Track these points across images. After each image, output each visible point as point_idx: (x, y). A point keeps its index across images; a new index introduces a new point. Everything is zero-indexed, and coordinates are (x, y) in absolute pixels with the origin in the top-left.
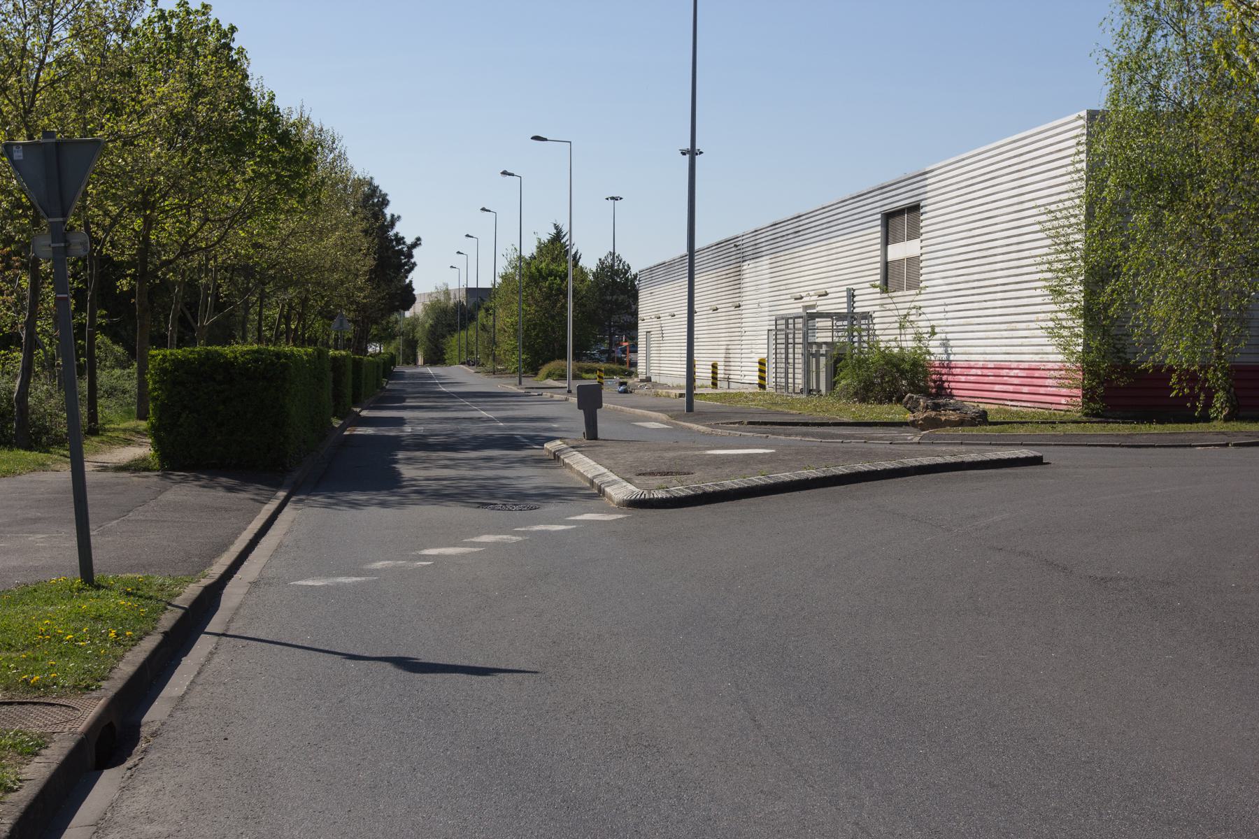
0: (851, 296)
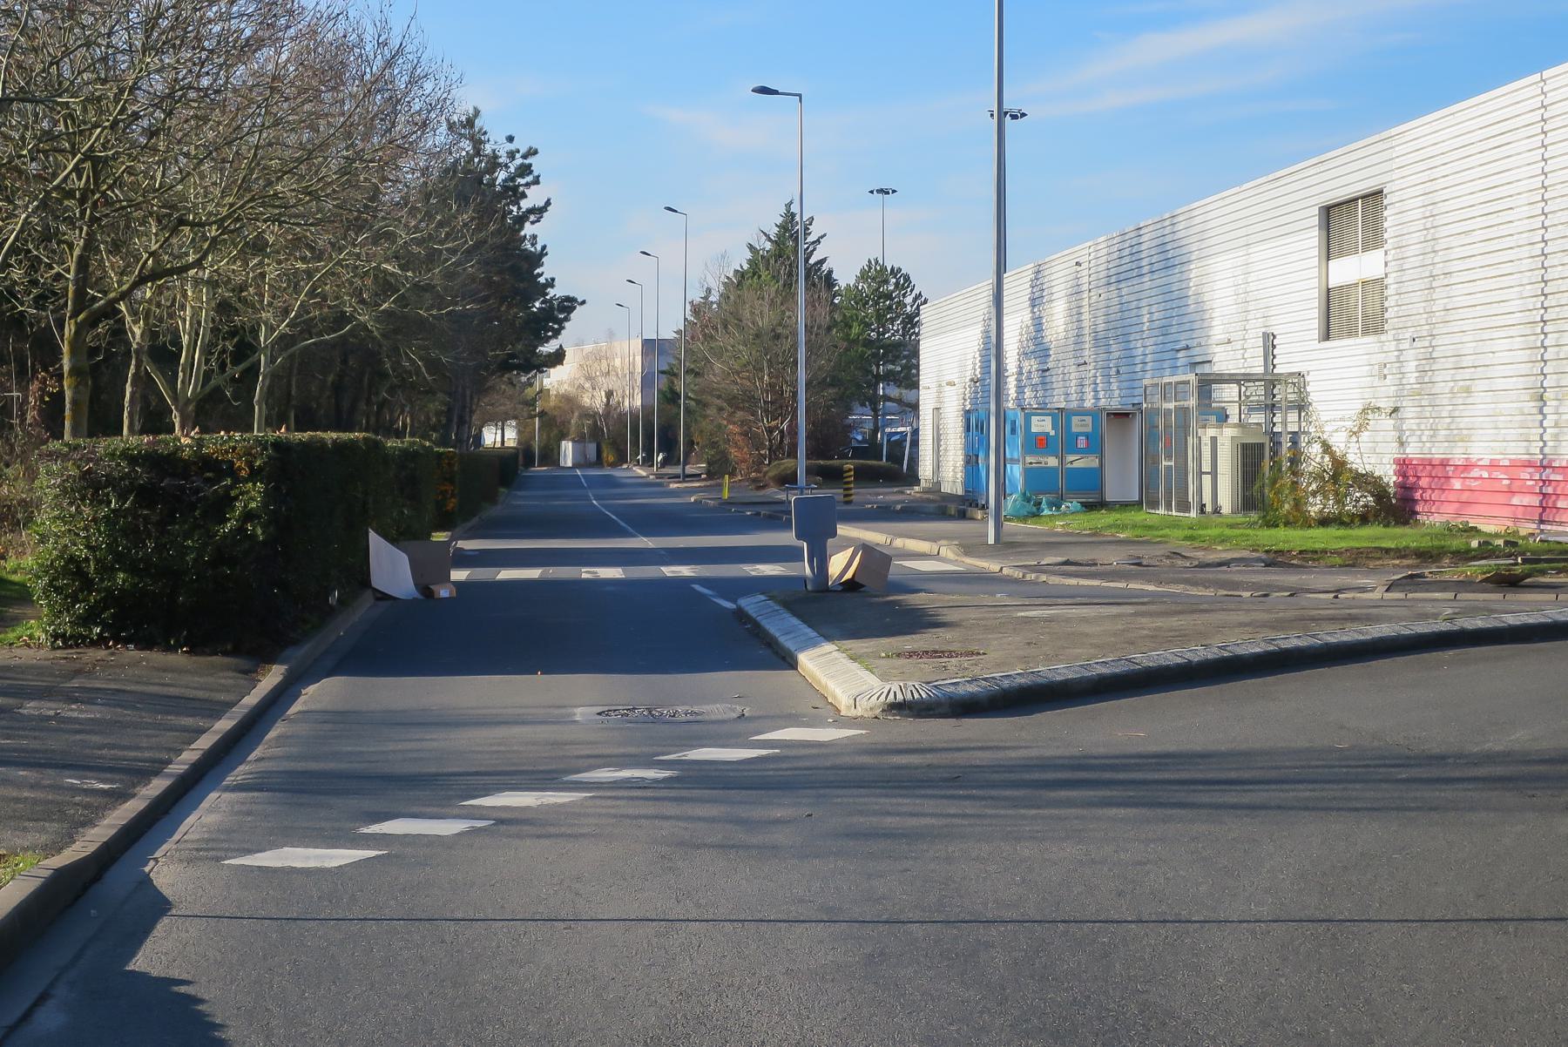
0: (1269, 342)
